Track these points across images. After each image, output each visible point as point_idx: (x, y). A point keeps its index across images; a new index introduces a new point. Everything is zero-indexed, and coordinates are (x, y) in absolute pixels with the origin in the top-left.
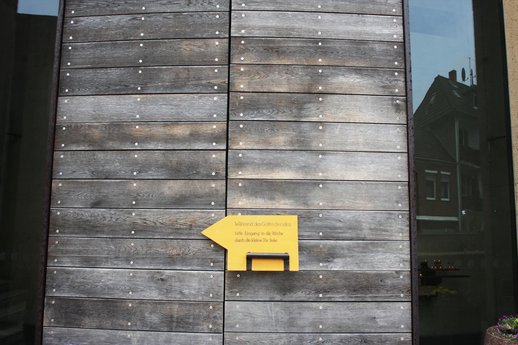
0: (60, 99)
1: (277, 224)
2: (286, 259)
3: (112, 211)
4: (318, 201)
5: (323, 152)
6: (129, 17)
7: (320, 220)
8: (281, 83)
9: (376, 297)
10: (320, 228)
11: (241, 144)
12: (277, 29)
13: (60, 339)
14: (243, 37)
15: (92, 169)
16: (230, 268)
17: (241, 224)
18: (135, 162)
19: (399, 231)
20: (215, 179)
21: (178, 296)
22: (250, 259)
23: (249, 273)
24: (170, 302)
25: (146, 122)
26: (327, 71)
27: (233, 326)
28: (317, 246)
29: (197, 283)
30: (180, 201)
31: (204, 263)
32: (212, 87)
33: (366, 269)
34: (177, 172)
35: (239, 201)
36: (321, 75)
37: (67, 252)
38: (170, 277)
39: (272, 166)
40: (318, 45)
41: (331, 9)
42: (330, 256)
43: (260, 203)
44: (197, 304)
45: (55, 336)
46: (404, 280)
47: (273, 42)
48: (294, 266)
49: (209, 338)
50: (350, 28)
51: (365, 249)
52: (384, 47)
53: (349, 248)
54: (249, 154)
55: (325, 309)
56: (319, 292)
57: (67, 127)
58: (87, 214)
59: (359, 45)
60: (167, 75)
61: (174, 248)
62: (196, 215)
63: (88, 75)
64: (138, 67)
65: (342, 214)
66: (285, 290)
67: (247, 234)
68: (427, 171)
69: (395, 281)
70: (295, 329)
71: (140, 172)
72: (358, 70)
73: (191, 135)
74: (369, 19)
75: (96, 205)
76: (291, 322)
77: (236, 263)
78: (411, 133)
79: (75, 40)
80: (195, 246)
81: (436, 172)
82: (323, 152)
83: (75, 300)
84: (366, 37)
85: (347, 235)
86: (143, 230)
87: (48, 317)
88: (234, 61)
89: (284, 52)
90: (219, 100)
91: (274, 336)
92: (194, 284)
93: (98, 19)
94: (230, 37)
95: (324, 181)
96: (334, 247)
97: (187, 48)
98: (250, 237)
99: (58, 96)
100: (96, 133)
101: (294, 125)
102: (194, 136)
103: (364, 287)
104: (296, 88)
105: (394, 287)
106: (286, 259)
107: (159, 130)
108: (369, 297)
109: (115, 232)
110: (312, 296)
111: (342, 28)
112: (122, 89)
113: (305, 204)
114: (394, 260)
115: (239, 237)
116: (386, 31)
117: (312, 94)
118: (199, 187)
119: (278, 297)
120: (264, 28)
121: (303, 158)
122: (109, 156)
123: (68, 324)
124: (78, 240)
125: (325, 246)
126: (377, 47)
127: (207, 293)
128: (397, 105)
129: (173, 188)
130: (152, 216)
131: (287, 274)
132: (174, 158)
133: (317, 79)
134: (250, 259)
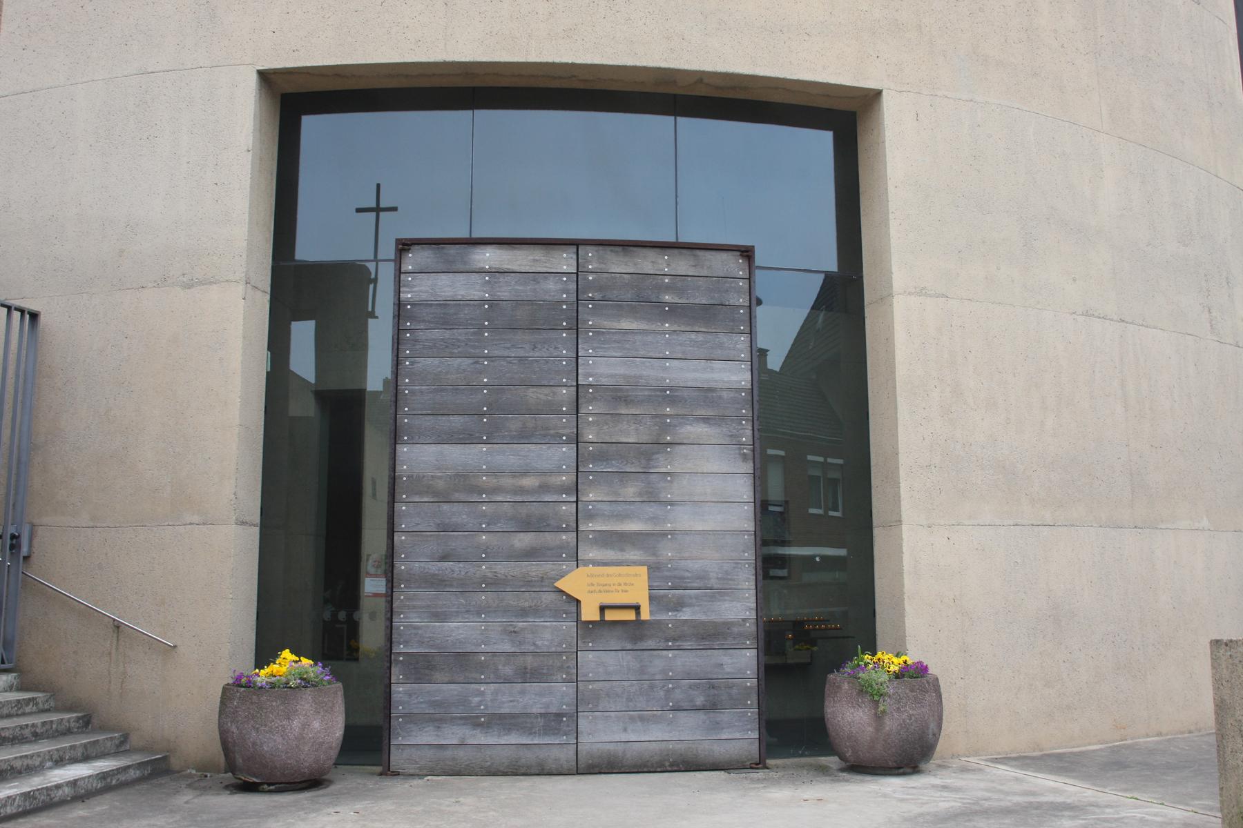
0: (398, 447)
1: (628, 575)
2: (637, 608)
3: (461, 565)
4: (667, 552)
5: (672, 503)
6: (470, 361)
7: (669, 570)
8: (630, 434)
9: (14, 505)
10: (667, 579)
11: (591, 496)
12: (625, 377)
13: (410, 695)
14: (590, 386)
15: (438, 521)
16: (584, 618)
17: (592, 576)
18: (484, 515)
19: (746, 581)
20: (565, 531)
21: (532, 648)
22: (603, 609)
23: (602, 623)
24: (523, 654)
25: (494, 473)
26: (675, 421)
27: (586, 676)
28: (666, 596)
29: (551, 633)
30: (531, 554)
31: (556, 614)
32: (561, 436)
33: (713, 617)
34: (526, 525)
35: (588, 553)
36: (670, 425)
37: (414, 607)
38: (523, 629)
39: (622, 517)
40: (667, 394)
41: (680, 356)
42: (679, 605)
43: (610, 554)
44: (550, 654)
45: (405, 693)
46: (750, 627)
47: (621, 390)
48: (645, 615)
49: (564, 688)
50: (698, 375)
51: (713, 598)
52: (732, 394)
53: (697, 597)
54: (599, 506)
55: (675, 657)
56: (668, 641)
57: (408, 477)
58: (434, 567)
59: (707, 394)
60: (514, 423)
61: (526, 601)
62: (547, 567)
63: (428, 422)
64: (483, 414)
65: (690, 564)
66: (636, 639)
67: (598, 585)
68: (810, 458)
69: (741, 629)
70: (646, 677)
71: (488, 524)
72: (705, 420)
73: (540, 487)
74: (717, 365)
75: (444, 558)
76: (642, 670)
77: (590, 613)
78: (758, 483)
79: (412, 384)
80: (548, 598)
81: (821, 459)
82: (672, 503)
83: (425, 655)
84: (714, 385)
85: (695, 585)
86: (495, 584)
87: (396, 674)
88: (582, 411)
89: (632, 401)
90: (567, 450)
91: (625, 683)
92: (548, 636)
93: (437, 361)
94: (577, 385)
95: (672, 532)
96: (682, 597)
97: (533, 395)
98: (602, 588)
99: (395, 439)
100: (441, 484)
101: (643, 476)
102: (544, 488)
103: (712, 636)
104: (645, 438)
105: (740, 635)
106: (637, 608)
107: (507, 481)
108: (716, 644)
109: (465, 586)
110: (662, 645)
111: (690, 375)
112: (467, 438)
113: (654, 554)
114: (740, 607)
115: (592, 588)
116: (734, 378)
117: (660, 445)
118: (549, 538)
119: (629, 646)
120: (612, 376)
121: (652, 509)
122: (456, 507)
123: (419, 680)
124: (425, 596)
125: (674, 595)
126: (725, 394)
127: (560, 644)
128: (744, 454)
129: (523, 540)
130: (503, 568)
131: (639, 623)
132: (523, 510)
133: (665, 428)
134: (603, 609)
